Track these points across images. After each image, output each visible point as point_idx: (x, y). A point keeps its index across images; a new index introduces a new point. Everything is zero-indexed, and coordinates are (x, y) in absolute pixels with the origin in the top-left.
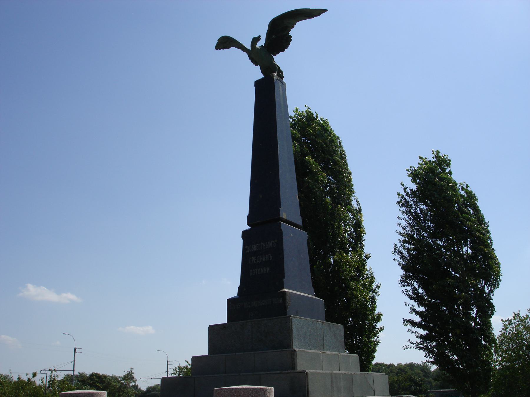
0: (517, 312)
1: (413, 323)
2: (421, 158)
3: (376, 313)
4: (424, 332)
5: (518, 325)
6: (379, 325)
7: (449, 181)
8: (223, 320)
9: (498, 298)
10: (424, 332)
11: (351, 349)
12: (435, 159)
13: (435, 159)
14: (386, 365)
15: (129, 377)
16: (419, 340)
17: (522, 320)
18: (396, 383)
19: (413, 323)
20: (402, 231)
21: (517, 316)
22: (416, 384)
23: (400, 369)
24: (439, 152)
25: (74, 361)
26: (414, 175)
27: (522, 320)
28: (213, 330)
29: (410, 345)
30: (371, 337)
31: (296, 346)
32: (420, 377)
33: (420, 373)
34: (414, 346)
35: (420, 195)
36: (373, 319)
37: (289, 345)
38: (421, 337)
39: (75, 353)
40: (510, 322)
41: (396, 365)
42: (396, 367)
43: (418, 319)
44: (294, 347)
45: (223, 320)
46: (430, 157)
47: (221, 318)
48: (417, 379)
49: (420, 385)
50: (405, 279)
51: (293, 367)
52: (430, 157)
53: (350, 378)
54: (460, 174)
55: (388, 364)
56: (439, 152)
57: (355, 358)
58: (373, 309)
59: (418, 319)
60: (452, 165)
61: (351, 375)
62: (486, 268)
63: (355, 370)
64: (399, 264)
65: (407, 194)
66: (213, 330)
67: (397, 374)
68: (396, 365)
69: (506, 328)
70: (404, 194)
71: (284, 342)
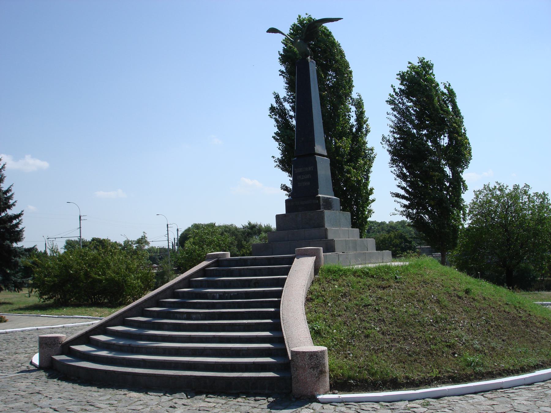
0: (486, 184)
1: (397, 195)
2: (409, 63)
3: (369, 188)
4: (407, 203)
5: (487, 194)
6: (371, 197)
7: (432, 81)
8: (283, 212)
9: (466, 175)
10: (407, 203)
11: (354, 225)
12: (420, 64)
13: (420, 64)
14: (378, 223)
15: (142, 241)
16: (404, 209)
17: (490, 190)
18: (388, 240)
19: (397, 195)
20: (392, 124)
21: (486, 187)
22: (406, 240)
23: (391, 227)
24: (424, 59)
25: (80, 228)
26: (402, 77)
27: (490, 190)
28: (278, 217)
29: (396, 212)
30: (365, 207)
31: (327, 226)
32: (410, 234)
33: (411, 231)
34: (399, 213)
35: (407, 93)
36: (367, 193)
37: (323, 226)
38: (405, 206)
39: (80, 220)
40: (481, 192)
41: (388, 223)
42: (387, 225)
43: (402, 192)
44: (326, 227)
45: (283, 212)
46: (416, 63)
47: (283, 211)
48: (408, 236)
49: (410, 242)
50: (393, 161)
51: (326, 237)
52: (416, 63)
53: (355, 242)
54: (441, 77)
55: (380, 222)
56: (424, 59)
57: (357, 230)
58: (366, 184)
59: (402, 192)
60: (434, 68)
61: (355, 240)
62: (459, 153)
63: (357, 238)
64: (388, 150)
65: (396, 93)
66: (278, 217)
67: (388, 232)
68: (388, 223)
69: (477, 197)
70: (394, 94)
71: (320, 224)
